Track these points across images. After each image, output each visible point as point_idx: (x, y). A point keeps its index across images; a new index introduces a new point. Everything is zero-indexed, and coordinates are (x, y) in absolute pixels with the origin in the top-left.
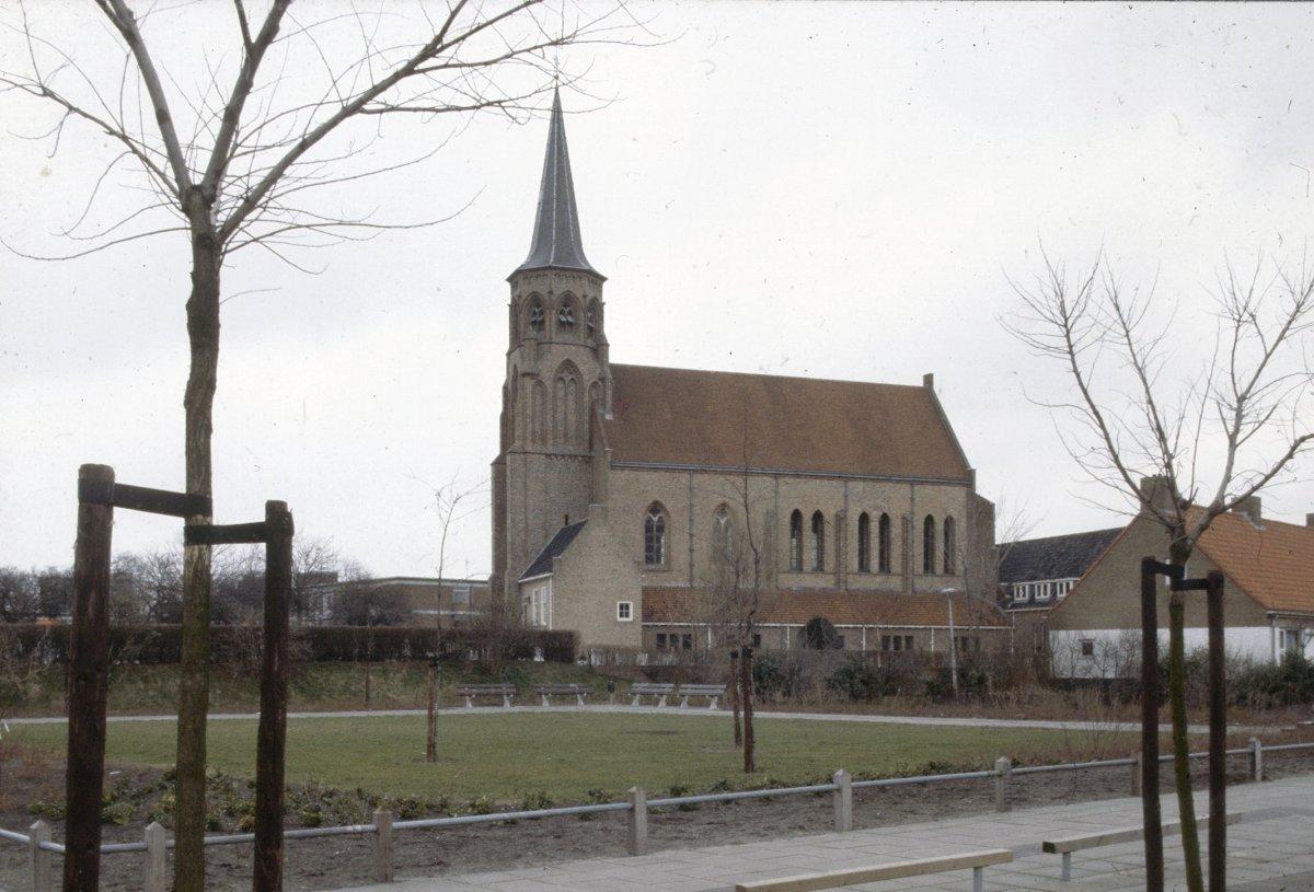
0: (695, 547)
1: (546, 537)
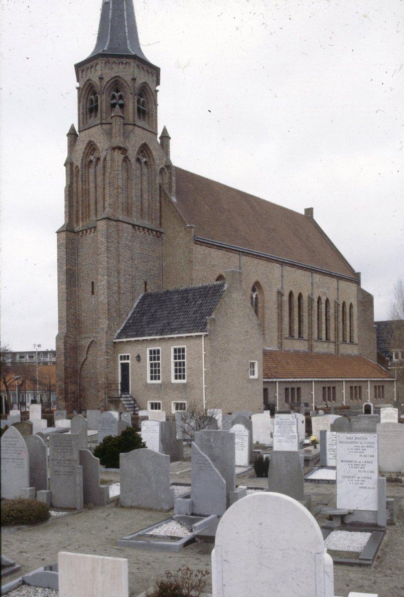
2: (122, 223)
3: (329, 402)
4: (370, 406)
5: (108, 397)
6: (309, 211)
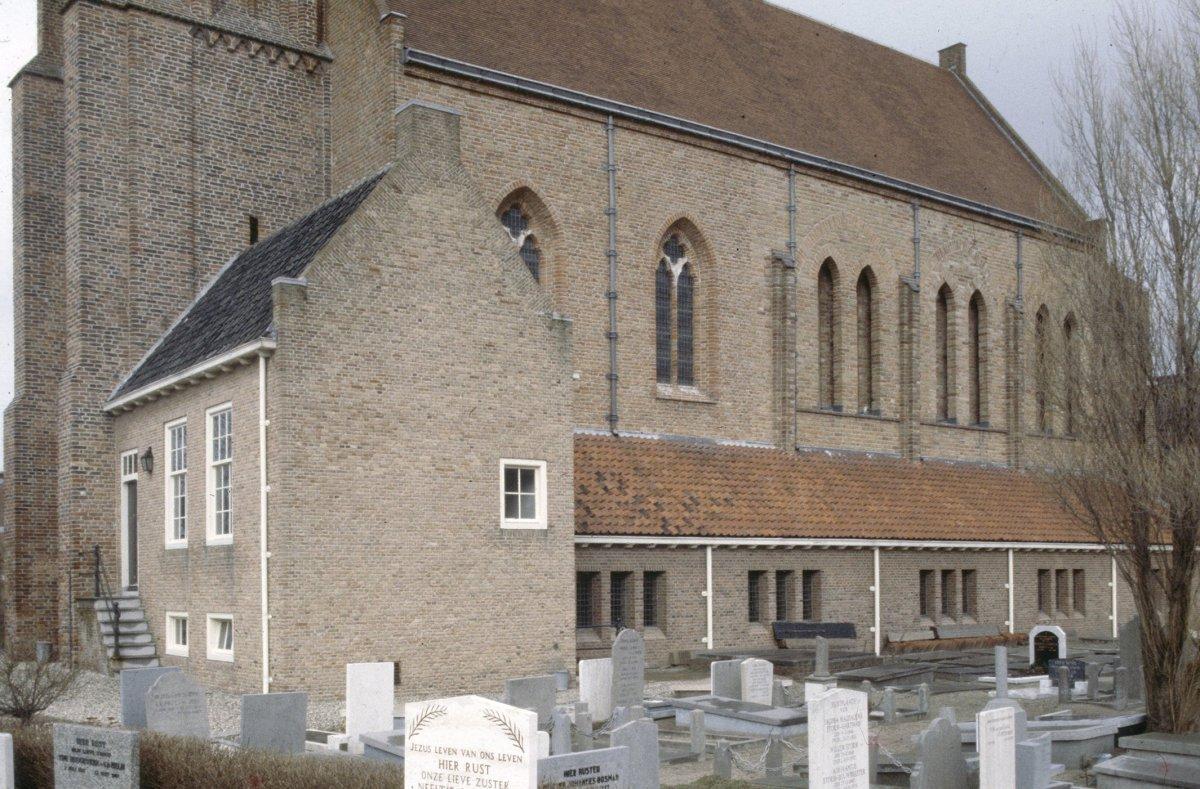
0: (621, 328)
1: (194, 272)
2: (145, 17)
3: (947, 622)
4: (1055, 640)
5: (78, 600)
6: (955, 54)
